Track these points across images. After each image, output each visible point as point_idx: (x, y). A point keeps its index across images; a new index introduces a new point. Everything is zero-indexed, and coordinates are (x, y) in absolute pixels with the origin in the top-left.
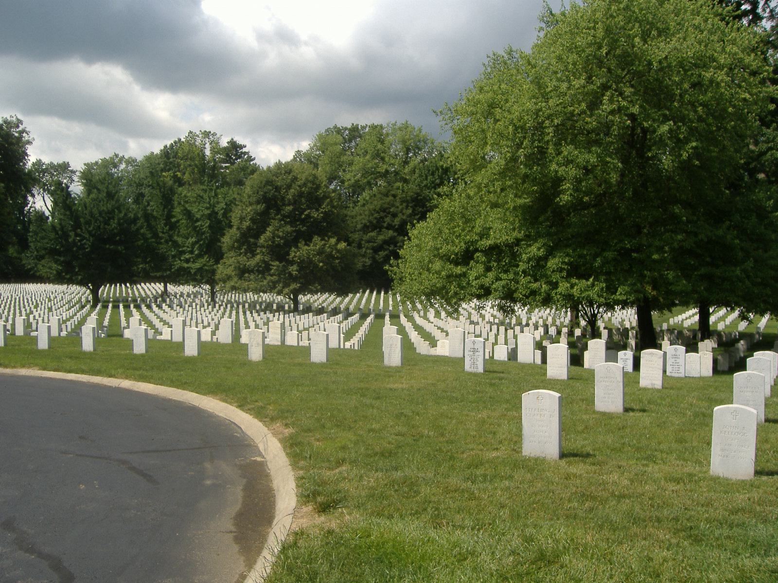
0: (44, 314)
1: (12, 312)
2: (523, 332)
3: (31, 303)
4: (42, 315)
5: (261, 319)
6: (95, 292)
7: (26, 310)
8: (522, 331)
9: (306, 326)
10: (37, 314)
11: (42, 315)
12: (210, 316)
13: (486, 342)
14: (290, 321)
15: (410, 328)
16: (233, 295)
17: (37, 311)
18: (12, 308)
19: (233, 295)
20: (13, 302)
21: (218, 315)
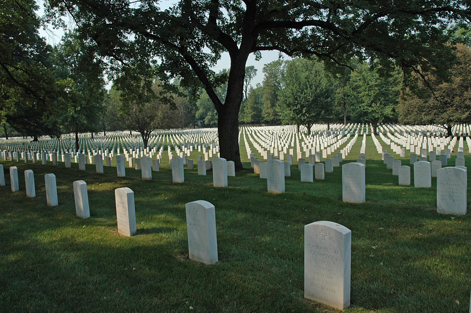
0: (316, 144)
1: (293, 139)
2: (402, 164)
3: (206, 139)
4: (314, 145)
5: (308, 140)
6: (309, 128)
7: (299, 138)
8: (437, 312)
9: (329, 144)
10: (307, 142)
11: (311, 143)
12: (284, 141)
13: (451, 142)
14: (320, 141)
15: (162, 238)
16: (464, 128)
17: (309, 137)
18: (293, 139)
19: (464, 128)
20: (197, 139)
21: (286, 139)
